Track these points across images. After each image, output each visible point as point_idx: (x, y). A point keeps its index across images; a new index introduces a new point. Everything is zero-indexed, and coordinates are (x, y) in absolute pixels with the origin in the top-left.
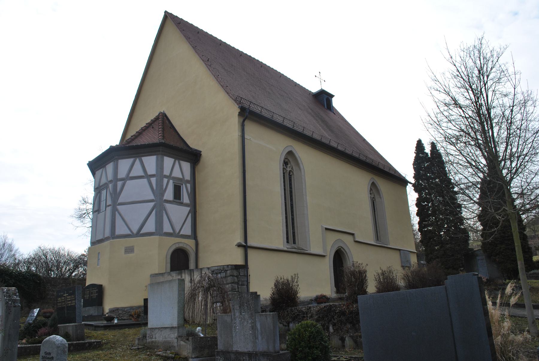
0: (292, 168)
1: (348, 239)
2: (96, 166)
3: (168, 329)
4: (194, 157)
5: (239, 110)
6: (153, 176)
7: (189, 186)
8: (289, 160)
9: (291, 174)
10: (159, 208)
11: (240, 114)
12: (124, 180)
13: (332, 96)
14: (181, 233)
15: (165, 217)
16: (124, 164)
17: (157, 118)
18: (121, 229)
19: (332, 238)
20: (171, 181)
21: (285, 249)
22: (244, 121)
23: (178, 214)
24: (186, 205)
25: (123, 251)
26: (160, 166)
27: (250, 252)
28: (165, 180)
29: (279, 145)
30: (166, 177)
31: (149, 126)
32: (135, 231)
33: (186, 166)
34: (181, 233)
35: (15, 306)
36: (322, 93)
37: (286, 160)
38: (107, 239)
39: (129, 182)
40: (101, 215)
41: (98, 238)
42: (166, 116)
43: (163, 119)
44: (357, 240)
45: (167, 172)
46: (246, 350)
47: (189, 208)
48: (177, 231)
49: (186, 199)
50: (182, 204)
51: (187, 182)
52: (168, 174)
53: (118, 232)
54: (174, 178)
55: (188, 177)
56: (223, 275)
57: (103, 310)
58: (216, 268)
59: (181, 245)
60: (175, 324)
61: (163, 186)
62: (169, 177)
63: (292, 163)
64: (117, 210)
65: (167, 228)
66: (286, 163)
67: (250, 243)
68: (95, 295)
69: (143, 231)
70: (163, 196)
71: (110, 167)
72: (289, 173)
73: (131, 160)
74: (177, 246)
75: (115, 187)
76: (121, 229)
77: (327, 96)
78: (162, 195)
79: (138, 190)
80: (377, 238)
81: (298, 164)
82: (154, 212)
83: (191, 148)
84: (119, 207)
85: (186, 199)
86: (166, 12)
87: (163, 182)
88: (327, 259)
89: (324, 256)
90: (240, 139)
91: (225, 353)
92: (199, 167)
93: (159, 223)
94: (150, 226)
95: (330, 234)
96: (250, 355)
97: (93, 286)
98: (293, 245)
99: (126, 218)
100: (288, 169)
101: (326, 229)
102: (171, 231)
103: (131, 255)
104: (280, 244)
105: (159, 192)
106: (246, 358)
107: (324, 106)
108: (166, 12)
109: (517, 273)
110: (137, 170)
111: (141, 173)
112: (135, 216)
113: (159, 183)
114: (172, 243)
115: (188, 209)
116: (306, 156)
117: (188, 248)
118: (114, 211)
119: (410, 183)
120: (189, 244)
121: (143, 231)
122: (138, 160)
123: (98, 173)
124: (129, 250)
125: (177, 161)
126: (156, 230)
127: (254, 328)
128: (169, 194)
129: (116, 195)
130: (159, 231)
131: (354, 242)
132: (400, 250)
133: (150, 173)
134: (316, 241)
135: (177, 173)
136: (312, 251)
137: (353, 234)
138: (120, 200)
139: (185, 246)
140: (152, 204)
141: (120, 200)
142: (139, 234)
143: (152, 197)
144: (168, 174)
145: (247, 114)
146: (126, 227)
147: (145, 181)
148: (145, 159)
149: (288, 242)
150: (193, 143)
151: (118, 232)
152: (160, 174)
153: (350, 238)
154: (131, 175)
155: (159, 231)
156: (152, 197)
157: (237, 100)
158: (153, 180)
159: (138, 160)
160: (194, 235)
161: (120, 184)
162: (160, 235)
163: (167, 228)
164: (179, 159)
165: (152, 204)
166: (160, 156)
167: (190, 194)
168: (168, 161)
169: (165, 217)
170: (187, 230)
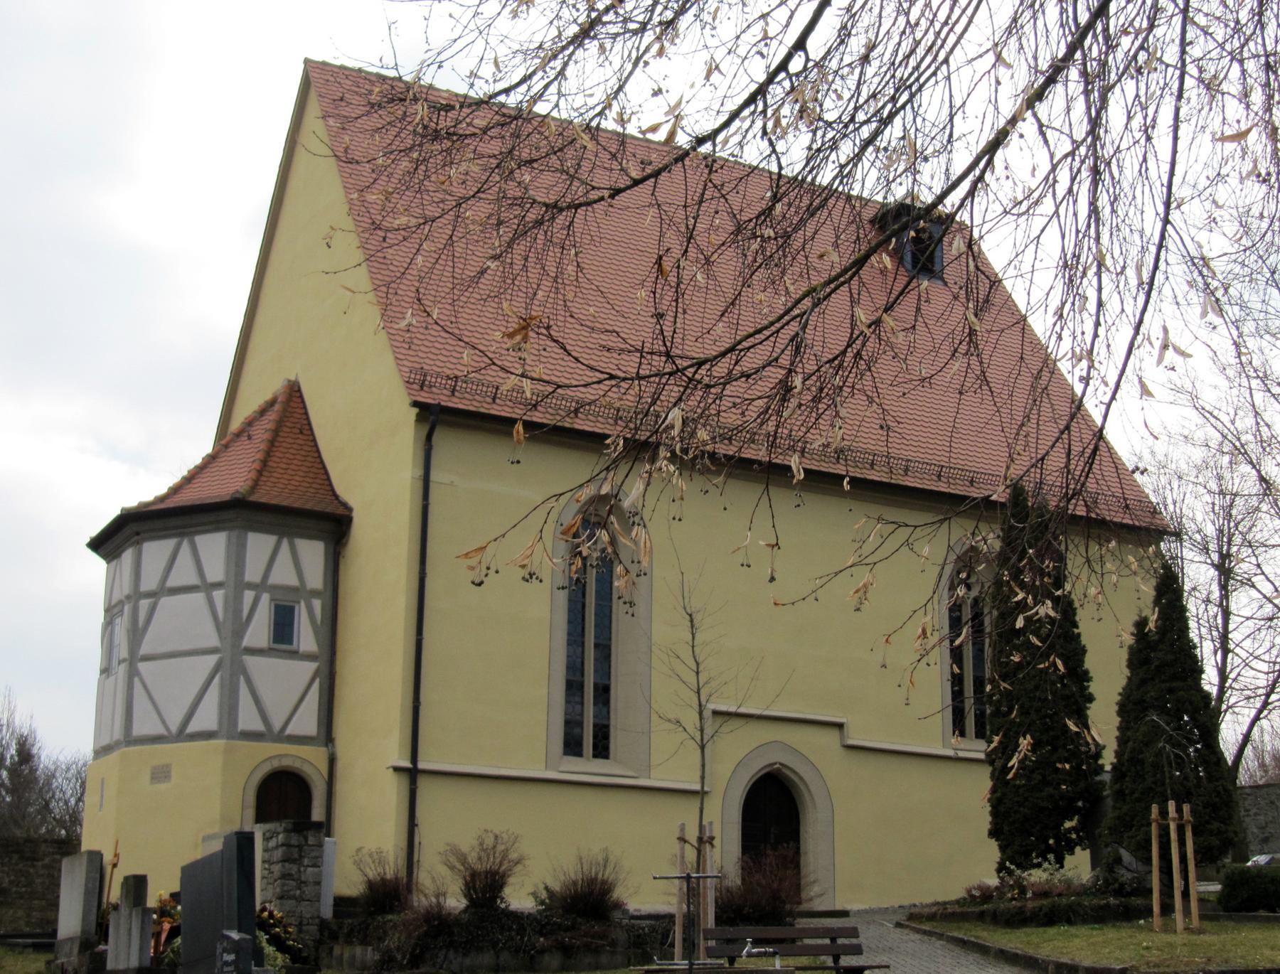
2: (108, 542)
6: (219, 585)
7: (317, 604)
10: (231, 668)
11: (420, 419)
14: (289, 731)
15: (244, 692)
22: (429, 438)
23: (283, 684)
24: (309, 657)
25: (147, 777)
26: (237, 559)
27: (424, 784)
28: (249, 595)
30: (250, 586)
32: (174, 728)
33: (313, 552)
34: (289, 731)
39: (166, 602)
40: (112, 679)
44: (850, 742)
45: (253, 573)
48: (277, 726)
49: (306, 638)
50: (294, 655)
51: (315, 593)
53: (139, 730)
54: (275, 588)
55: (315, 577)
59: (286, 763)
61: (241, 611)
65: (248, 719)
69: (192, 728)
74: (276, 764)
75: (135, 611)
76: (145, 724)
78: (239, 632)
79: (187, 621)
82: (217, 680)
84: (142, 666)
85: (306, 638)
86: (307, 61)
87: (241, 603)
90: (420, 484)
93: (229, 708)
94: (207, 718)
102: (258, 726)
103: (162, 787)
105: (234, 626)
108: (307, 62)
111: (193, 580)
112: (179, 687)
113: (234, 602)
115: (313, 666)
117: (308, 771)
118: (133, 673)
120: (311, 760)
121: (192, 728)
122: (185, 546)
124: (161, 774)
125: (285, 542)
126: (220, 723)
128: (259, 632)
130: (229, 728)
131: (842, 750)
135: (283, 574)
137: (840, 726)
138: (145, 649)
139: (297, 764)
140: (212, 660)
141: (145, 649)
142: (182, 735)
143: (214, 641)
147: (199, 597)
148: (200, 540)
149: (572, 746)
152: (237, 582)
153: (831, 737)
155: (229, 728)
156: (214, 641)
158: (218, 595)
159: (185, 546)
161: (144, 604)
162: (230, 737)
163: (248, 719)
165: (212, 660)
166: (235, 533)
167: (311, 627)
168: (259, 545)
169: (244, 692)
170: (307, 722)
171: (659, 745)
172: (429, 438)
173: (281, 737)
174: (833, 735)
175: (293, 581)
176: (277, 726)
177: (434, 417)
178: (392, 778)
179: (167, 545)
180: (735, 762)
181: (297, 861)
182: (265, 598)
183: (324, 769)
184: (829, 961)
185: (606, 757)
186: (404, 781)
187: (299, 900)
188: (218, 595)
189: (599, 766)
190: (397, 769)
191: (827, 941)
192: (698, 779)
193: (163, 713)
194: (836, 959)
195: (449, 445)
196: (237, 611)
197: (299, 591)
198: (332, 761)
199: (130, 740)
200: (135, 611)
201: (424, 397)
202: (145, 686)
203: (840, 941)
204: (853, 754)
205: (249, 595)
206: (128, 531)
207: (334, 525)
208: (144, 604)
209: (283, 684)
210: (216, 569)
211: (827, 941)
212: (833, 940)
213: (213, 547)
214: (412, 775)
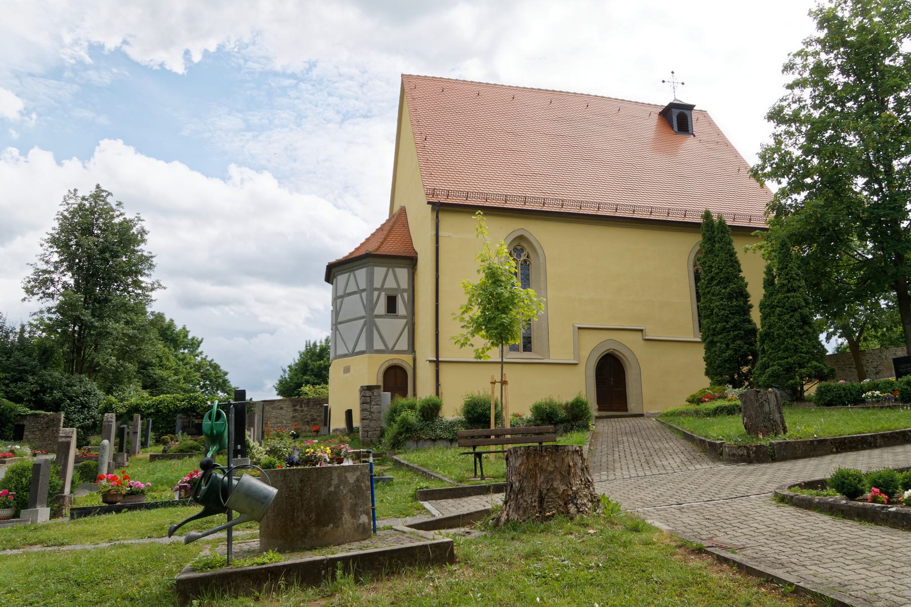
6: (364, 290)
7: (406, 295)
10: (370, 325)
11: (433, 210)
12: (342, 297)
14: (395, 349)
22: (437, 217)
26: (370, 280)
27: (441, 366)
28: (376, 293)
30: (376, 289)
33: (403, 273)
34: (395, 349)
39: (346, 299)
45: (377, 284)
47: (405, 321)
48: (390, 347)
55: (404, 284)
59: (395, 362)
65: (378, 345)
74: (391, 363)
77: (679, 111)
78: (373, 309)
79: (354, 306)
85: (401, 309)
88: (581, 369)
93: (370, 341)
94: (362, 346)
95: (586, 335)
102: (382, 347)
105: (370, 307)
107: (672, 128)
109: (407, 393)
111: (356, 289)
113: (370, 297)
114: (384, 360)
116: (537, 231)
117: (404, 365)
119: (745, 232)
120: (405, 360)
128: (381, 307)
131: (643, 342)
135: (391, 284)
137: (641, 331)
139: (400, 362)
140: (362, 321)
142: (354, 354)
143: (364, 314)
152: (370, 288)
156: (364, 314)
158: (364, 294)
164: (393, 267)
165: (362, 321)
168: (379, 272)
169: (709, 549)
170: (403, 345)
171: (559, 344)
172: (437, 217)
173: (392, 351)
175: (395, 286)
176: (390, 347)
177: (440, 208)
179: (346, 275)
180: (591, 349)
181: (369, 403)
182: (383, 294)
183: (412, 365)
185: (530, 351)
186: (433, 365)
187: (371, 420)
188: (364, 294)
189: (527, 355)
190: (430, 361)
192: (434, 355)
195: (449, 222)
198: (415, 360)
201: (435, 200)
204: (649, 342)
205: (376, 293)
207: (411, 261)
208: (339, 301)
211: (537, 444)
213: (361, 274)
214: (437, 363)
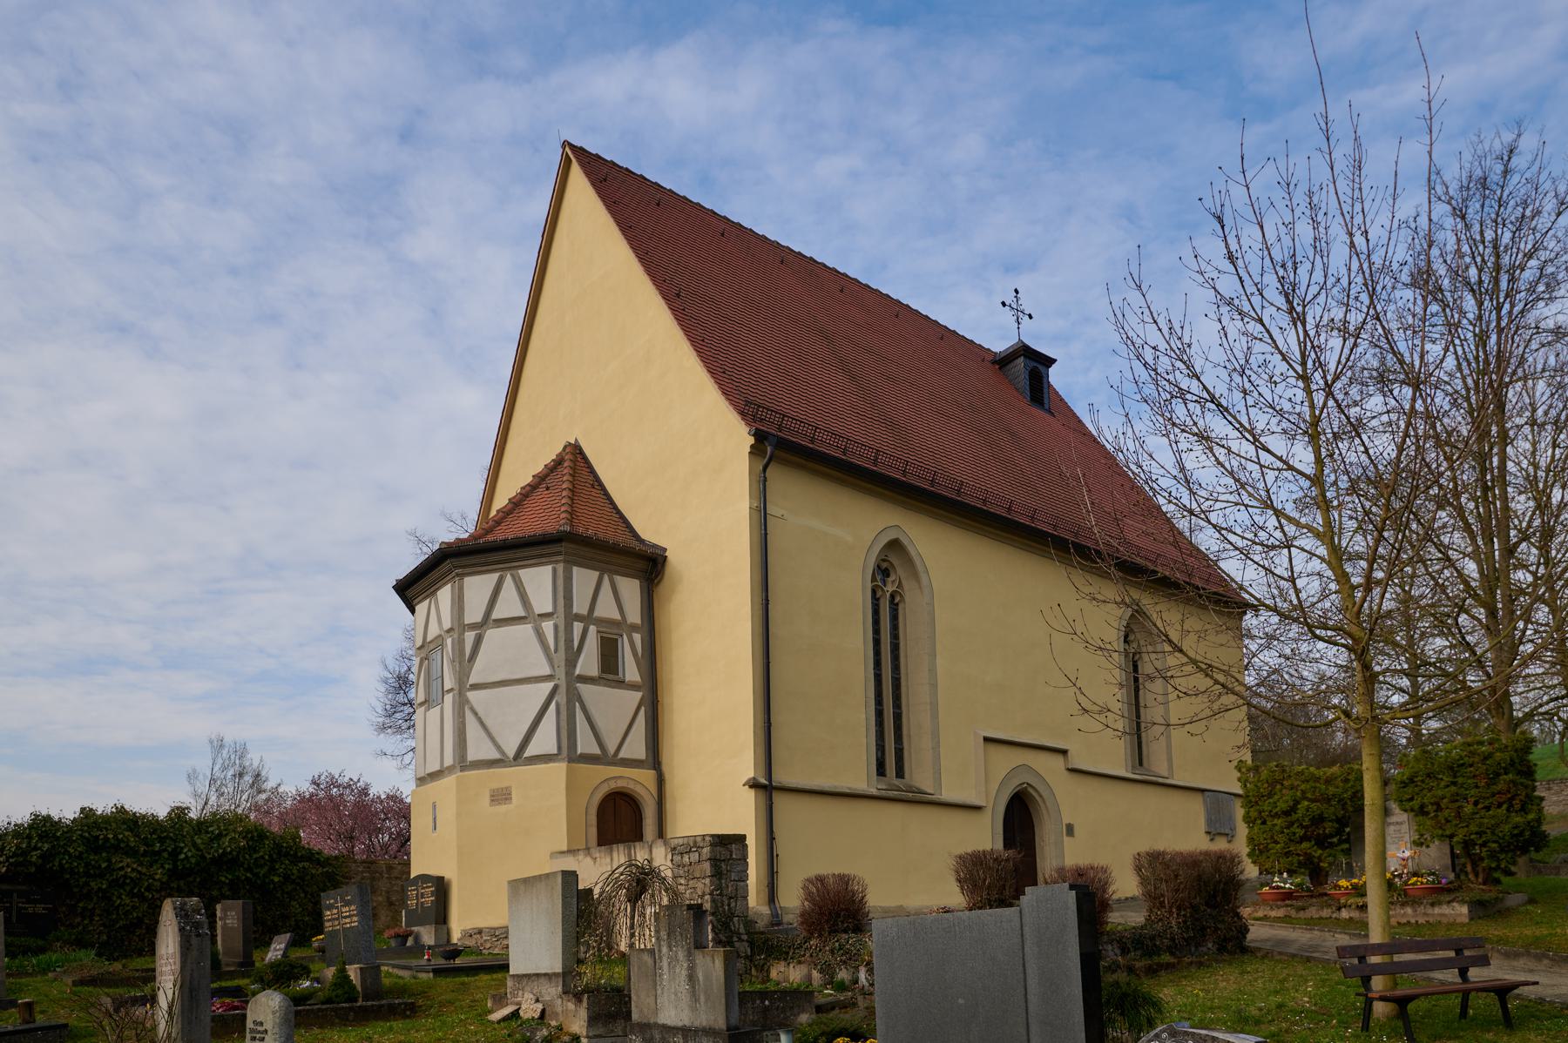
0: (900, 585)
1: (1049, 767)
2: (411, 588)
3: (542, 980)
4: (649, 565)
5: (751, 440)
7: (637, 637)
8: (891, 562)
9: (897, 599)
10: (568, 697)
11: (755, 451)
13: (1050, 362)
14: (622, 755)
16: (478, 587)
17: (558, 462)
18: (479, 748)
19: (1007, 760)
20: (592, 629)
21: (874, 791)
23: (614, 708)
24: (633, 687)
26: (564, 593)
27: (780, 800)
28: (578, 627)
29: (859, 525)
30: (578, 618)
31: (540, 480)
32: (511, 751)
33: (630, 589)
34: (622, 755)
35: (198, 935)
36: (1023, 351)
37: (885, 565)
38: (451, 769)
39: (492, 635)
41: (430, 770)
42: (581, 452)
43: (574, 461)
45: (580, 607)
46: (680, 1024)
48: (611, 749)
49: (631, 672)
50: (621, 684)
51: (634, 628)
52: (585, 612)
53: (472, 756)
54: (600, 622)
55: (634, 615)
56: (695, 857)
57: (449, 933)
58: (681, 841)
59: (621, 784)
60: (559, 970)
62: (588, 619)
63: (900, 571)
64: (468, 701)
65: (586, 744)
66: (883, 571)
67: (782, 777)
68: (429, 900)
70: (575, 666)
71: (445, 594)
72: (893, 596)
73: (496, 576)
74: (613, 785)
75: (460, 643)
76: (479, 748)
78: (571, 662)
79: (515, 651)
80: (1139, 756)
81: (915, 575)
82: (553, 706)
83: (642, 541)
84: (471, 695)
85: (631, 672)
88: (987, 815)
89: (978, 808)
91: (645, 1028)
92: (662, 589)
93: (567, 734)
94: (546, 740)
96: (685, 1031)
97: (424, 878)
98: (897, 782)
99: (488, 723)
100: (890, 588)
101: (986, 739)
103: (503, 808)
104: (860, 777)
106: (679, 1039)
110: (508, 605)
111: (519, 611)
114: (604, 778)
115: (638, 695)
118: (462, 704)
120: (641, 781)
123: (421, 608)
124: (501, 796)
127: (691, 978)
128: (589, 663)
129: (465, 662)
132: (1203, 791)
133: (538, 610)
134: (963, 771)
136: (947, 795)
137: (1064, 752)
139: (631, 786)
140: (547, 687)
144: (585, 612)
145: (781, 447)
146: (490, 744)
147: (527, 629)
148: (524, 574)
149: (881, 770)
150: (649, 529)
151: (472, 756)
153: (1057, 762)
154: (495, 615)
156: (547, 671)
157: (748, 410)
158: (548, 627)
160: (655, 758)
161: (470, 637)
163: (586, 744)
164: (612, 572)
167: (635, 659)
168: (584, 579)
170: (636, 748)
174: (1059, 759)
176: (611, 749)
178: (751, 795)
183: (653, 788)
184: (1451, 976)
191: (1452, 954)
193: (498, 739)
194: (1463, 973)
196: (569, 640)
197: (620, 624)
198: (661, 781)
199: (463, 763)
200: (460, 643)
202: (476, 714)
203: (1467, 953)
205: (578, 627)
206: (446, 565)
209: (614, 708)
210: (543, 601)
212: (1459, 952)
213: (539, 580)
